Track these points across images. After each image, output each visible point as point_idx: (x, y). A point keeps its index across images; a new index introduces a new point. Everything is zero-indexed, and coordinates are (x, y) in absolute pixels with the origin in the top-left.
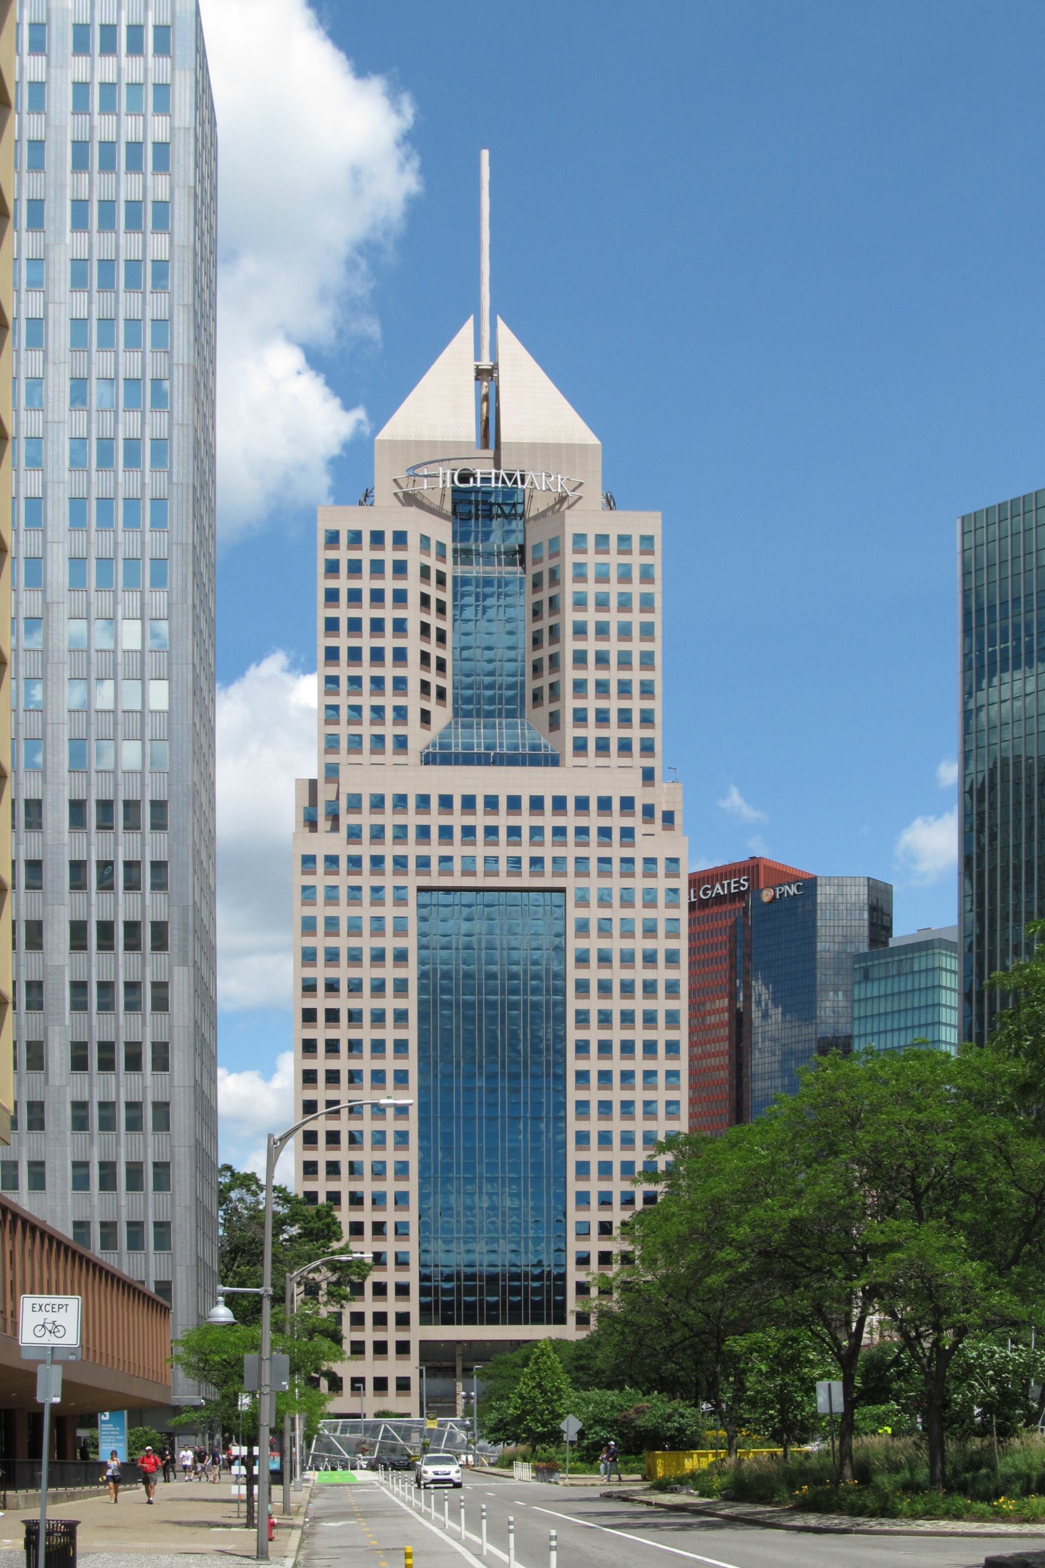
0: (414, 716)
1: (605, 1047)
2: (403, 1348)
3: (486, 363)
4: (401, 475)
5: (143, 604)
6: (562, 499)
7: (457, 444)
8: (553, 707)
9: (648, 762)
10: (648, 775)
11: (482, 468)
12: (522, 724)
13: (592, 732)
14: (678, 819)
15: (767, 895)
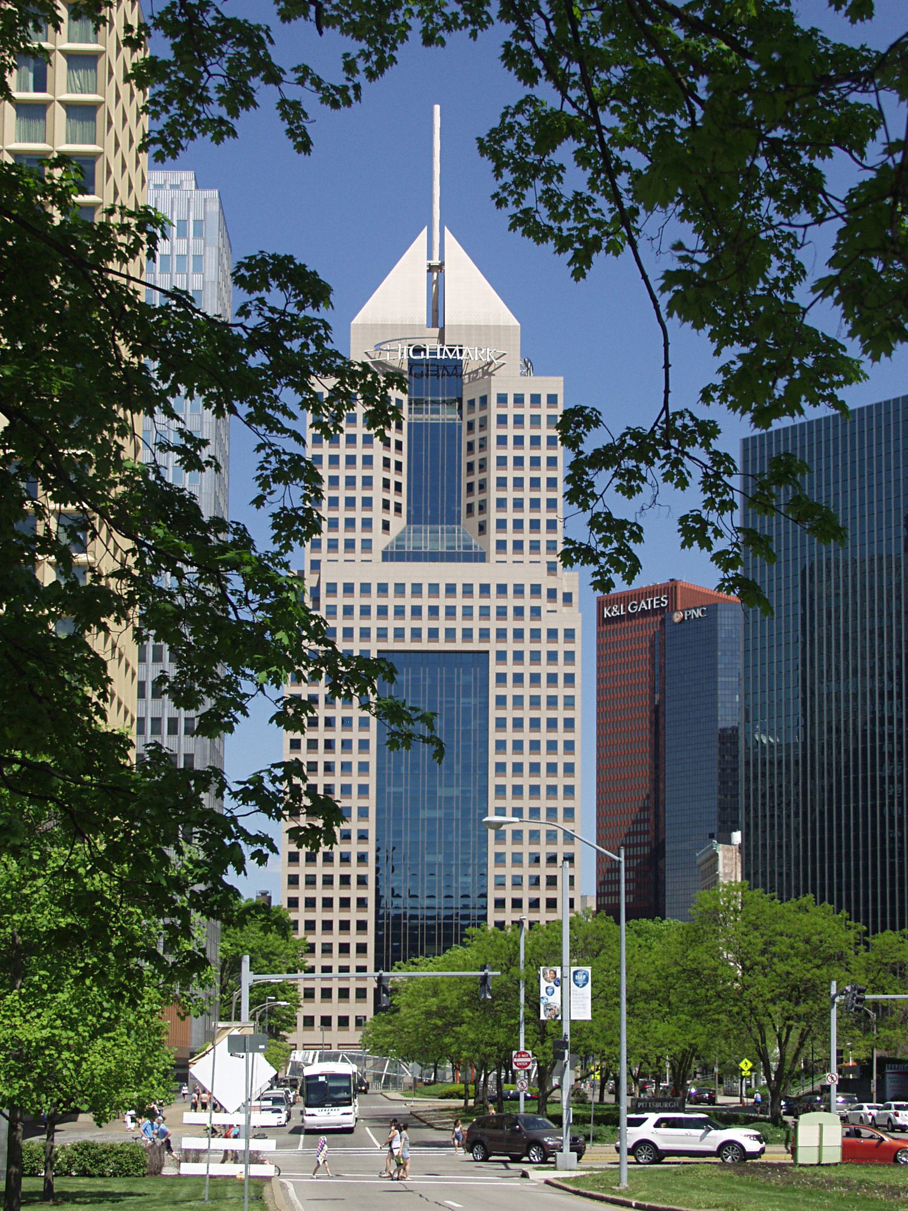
0: (377, 525)
3: (436, 261)
4: (371, 350)
6: (490, 364)
7: (412, 327)
8: (482, 518)
11: (431, 344)
13: (510, 536)
14: (575, 598)
15: (677, 617)
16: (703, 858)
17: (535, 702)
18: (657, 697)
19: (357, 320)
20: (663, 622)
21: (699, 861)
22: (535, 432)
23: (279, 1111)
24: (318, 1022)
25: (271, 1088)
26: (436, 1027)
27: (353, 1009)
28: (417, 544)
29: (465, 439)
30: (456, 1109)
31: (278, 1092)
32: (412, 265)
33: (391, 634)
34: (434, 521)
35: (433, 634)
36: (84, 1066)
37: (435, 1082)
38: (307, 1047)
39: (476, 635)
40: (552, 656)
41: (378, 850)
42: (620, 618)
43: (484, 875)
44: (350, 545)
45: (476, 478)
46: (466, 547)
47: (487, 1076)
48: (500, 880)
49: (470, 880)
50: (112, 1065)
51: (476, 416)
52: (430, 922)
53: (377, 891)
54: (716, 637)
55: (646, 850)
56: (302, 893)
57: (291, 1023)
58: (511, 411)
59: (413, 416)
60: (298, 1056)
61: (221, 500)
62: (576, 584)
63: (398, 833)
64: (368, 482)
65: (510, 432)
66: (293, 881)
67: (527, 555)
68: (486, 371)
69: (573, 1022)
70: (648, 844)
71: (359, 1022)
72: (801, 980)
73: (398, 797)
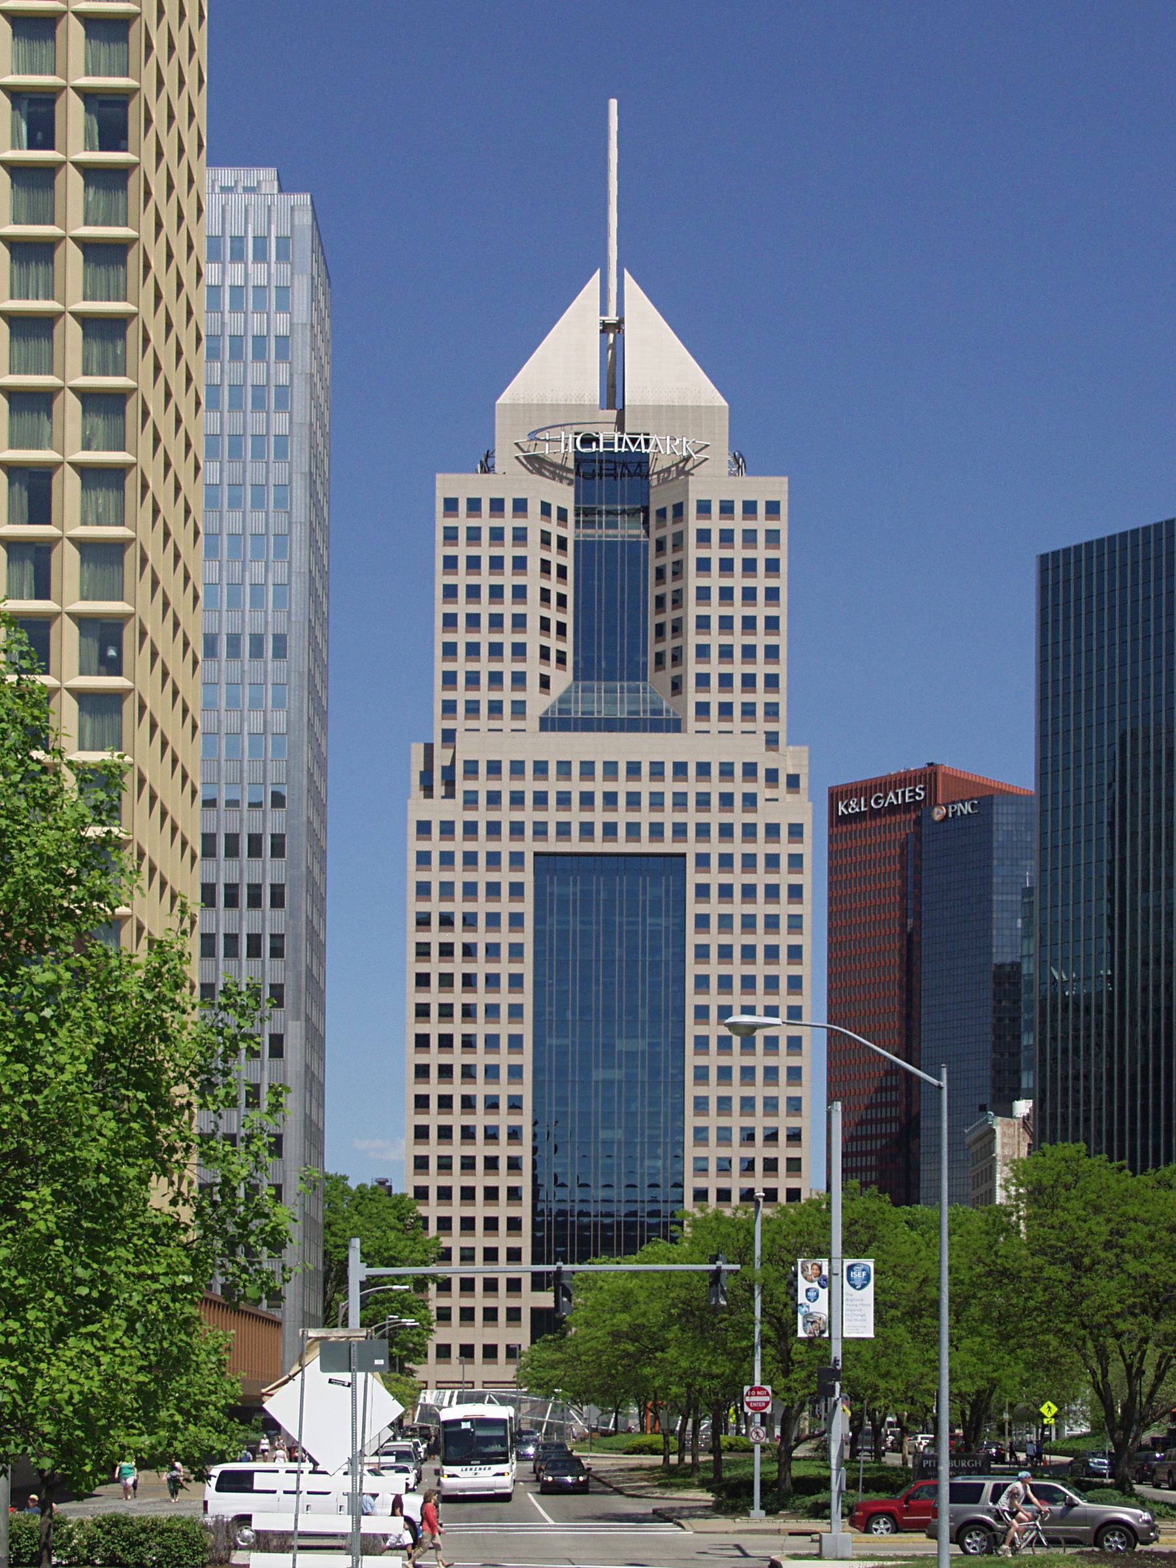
0: (533, 682)
1: (725, 952)
2: (514, 1315)
3: (612, 318)
4: (523, 440)
5: (265, 722)
6: (687, 459)
8: (677, 671)
9: (771, 727)
10: (772, 740)
11: (606, 432)
12: (645, 689)
13: (714, 697)
14: (804, 783)
15: (938, 813)
16: (976, 1134)
17: (749, 923)
18: (910, 922)
19: (504, 399)
20: (918, 822)
21: (967, 1140)
22: (749, 554)
23: (406, 1470)
24: (455, 1352)
25: (394, 1438)
26: (628, 1355)
27: (502, 1335)
28: (588, 708)
29: (653, 563)
30: (652, 1468)
31: (404, 1444)
32: (579, 322)
33: (552, 830)
34: (610, 676)
35: (610, 830)
36: (39, 1385)
37: (616, 1433)
38: (441, 1385)
39: (668, 832)
40: (772, 861)
41: (535, 1123)
42: (860, 816)
43: (679, 1158)
44: (496, 708)
45: (668, 616)
46: (654, 712)
47: (696, 1425)
48: (701, 1164)
49: (660, 1163)
50: (95, 1385)
51: (669, 530)
52: (607, 1221)
53: (535, 1178)
54: (990, 842)
55: (894, 1128)
56: (433, 1180)
57: (419, 1353)
58: (715, 524)
59: (582, 531)
60: (429, 1397)
61: (318, 633)
62: (806, 762)
63: (562, 1100)
64: (519, 622)
65: (715, 553)
66: (421, 1164)
67: (737, 723)
68: (682, 469)
69: (845, 1341)
70: (897, 1119)
71: (512, 1352)
72: (1165, 1284)
73: (562, 1052)
